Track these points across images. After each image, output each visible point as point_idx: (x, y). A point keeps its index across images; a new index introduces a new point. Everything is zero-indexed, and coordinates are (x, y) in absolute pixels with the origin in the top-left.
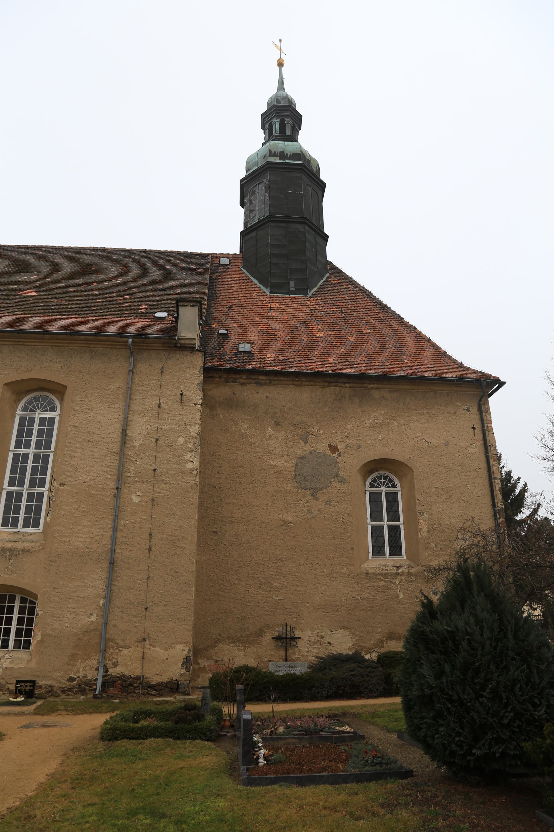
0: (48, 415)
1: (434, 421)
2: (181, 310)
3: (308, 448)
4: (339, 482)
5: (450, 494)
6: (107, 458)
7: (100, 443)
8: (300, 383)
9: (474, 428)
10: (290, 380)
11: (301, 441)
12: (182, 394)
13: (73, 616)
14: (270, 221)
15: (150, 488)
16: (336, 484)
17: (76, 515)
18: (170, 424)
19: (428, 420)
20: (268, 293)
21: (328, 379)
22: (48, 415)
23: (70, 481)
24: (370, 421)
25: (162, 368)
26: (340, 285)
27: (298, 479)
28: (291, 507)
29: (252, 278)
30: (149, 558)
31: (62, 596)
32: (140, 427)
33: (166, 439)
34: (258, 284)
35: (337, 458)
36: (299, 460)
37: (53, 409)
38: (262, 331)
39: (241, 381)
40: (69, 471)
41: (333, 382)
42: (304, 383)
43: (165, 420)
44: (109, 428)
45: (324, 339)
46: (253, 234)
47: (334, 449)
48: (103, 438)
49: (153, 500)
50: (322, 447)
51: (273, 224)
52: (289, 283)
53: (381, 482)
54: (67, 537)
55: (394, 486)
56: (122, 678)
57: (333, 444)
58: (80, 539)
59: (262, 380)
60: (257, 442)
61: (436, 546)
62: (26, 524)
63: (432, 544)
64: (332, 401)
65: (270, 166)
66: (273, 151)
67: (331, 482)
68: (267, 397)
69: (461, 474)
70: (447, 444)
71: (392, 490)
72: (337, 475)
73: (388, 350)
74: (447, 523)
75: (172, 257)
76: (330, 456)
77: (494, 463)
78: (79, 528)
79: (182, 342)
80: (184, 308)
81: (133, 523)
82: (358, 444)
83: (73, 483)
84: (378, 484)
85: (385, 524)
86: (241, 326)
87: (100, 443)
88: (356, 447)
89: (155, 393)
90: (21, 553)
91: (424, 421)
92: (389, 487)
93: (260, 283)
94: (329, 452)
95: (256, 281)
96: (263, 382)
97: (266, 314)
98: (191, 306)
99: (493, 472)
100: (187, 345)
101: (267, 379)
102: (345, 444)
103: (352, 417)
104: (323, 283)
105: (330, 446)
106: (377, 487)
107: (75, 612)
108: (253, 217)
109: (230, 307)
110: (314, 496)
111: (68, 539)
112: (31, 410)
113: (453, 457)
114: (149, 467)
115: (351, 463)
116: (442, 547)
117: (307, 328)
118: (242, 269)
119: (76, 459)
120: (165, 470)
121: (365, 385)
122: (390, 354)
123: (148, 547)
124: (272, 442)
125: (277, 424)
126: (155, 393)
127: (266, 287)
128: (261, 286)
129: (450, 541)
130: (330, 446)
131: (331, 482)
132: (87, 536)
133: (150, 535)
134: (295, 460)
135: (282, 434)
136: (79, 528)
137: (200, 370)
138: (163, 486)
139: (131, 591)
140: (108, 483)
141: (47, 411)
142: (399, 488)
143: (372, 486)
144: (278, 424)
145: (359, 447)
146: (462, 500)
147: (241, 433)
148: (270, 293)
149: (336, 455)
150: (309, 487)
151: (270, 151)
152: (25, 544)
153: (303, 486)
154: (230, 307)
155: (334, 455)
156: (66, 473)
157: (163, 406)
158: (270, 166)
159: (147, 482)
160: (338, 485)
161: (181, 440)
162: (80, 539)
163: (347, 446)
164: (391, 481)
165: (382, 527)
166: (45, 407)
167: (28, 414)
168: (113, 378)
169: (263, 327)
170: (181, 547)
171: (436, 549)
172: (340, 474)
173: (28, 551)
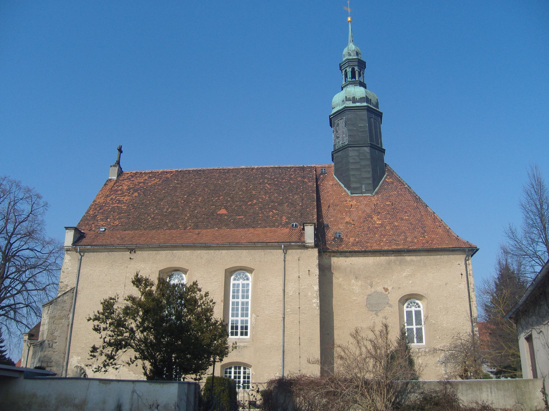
0: (246, 282)
1: (440, 271)
2: (306, 227)
3: (373, 290)
4: (389, 307)
5: (447, 311)
6: (277, 303)
7: (273, 296)
8: (367, 255)
9: (462, 274)
10: (362, 254)
11: (369, 286)
12: (309, 271)
13: (268, 374)
14: (349, 147)
15: (298, 316)
16: (387, 308)
17: (265, 330)
18: (304, 285)
19: (436, 271)
20: (350, 194)
21: (382, 253)
22: (246, 282)
23: (261, 315)
24: (405, 274)
25: (299, 258)
26: (392, 183)
27: (368, 306)
28: (365, 321)
29: (340, 183)
30: (125, 283)
31: (263, 366)
32: (291, 289)
33: (303, 293)
34: (344, 187)
35: (388, 294)
36: (368, 297)
37: (248, 279)
38: (347, 222)
39: (337, 256)
40: (260, 310)
41: (385, 254)
42: (369, 255)
43: (302, 283)
44: (276, 288)
45: (382, 225)
46: (339, 154)
47: (386, 290)
48: (274, 294)
49: (299, 322)
50: (380, 289)
51: (350, 149)
52: (362, 187)
53: (412, 305)
54: (262, 340)
55: (419, 307)
56: (321, 373)
57: (386, 287)
58: (268, 341)
59: (348, 255)
60: (347, 288)
61: (439, 338)
62: (242, 334)
63: (438, 337)
64: (385, 264)
65: (346, 109)
66: (348, 97)
67: (385, 307)
68: (351, 264)
69: (453, 300)
70: (446, 284)
71: (418, 309)
72: (388, 303)
73: (417, 230)
74: (445, 326)
75: (293, 171)
76: (384, 293)
77: (472, 293)
78: (267, 336)
79: (307, 244)
80: (307, 226)
81: (291, 332)
82: (399, 287)
83: (263, 315)
84: (411, 306)
85: (414, 327)
86: (335, 220)
87: (273, 296)
88: (397, 288)
89: (296, 271)
90: (243, 347)
91: (434, 272)
92: (416, 307)
93: (345, 187)
94: (384, 292)
95: (343, 185)
96: (348, 256)
97: (349, 210)
98: (310, 225)
99: (472, 298)
100: (310, 246)
101: (350, 255)
102: (392, 287)
103: (396, 272)
104: (383, 183)
105: (384, 288)
106: (410, 308)
107: (269, 373)
108: (339, 142)
109: (329, 206)
110: (376, 314)
111: (263, 341)
112: (237, 280)
113: (450, 291)
114: (296, 306)
115: (394, 297)
116: (443, 338)
117: (372, 218)
118: (334, 176)
119: (263, 304)
120: (304, 308)
121: (402, 254)
122: (418, 233)
123: (299, 343)
124: (355, 287)
125: (356, 278)
126: (296, 271)
127: (349, 190)
128: (346, 189)
129: (447, 335)
130: (384, 288)
131: (385, 307)
132: (271, 339)
133: (300, 338)
134: (366, 296)
135: (360, 283)
136: (267, 336)
137: (317, 257)
138: (304, 315)
139: (293, 363)
140: (278, 315)
141: (245, 280)
142: (422, 307)
143: (407, 307)
144: (357, 278)
145: (399, 288)
146: (454, 314)
147: (338, 283)
148: (352, 194)
149: (387, 293)
150: (374, 310)
151: (346, 97)
152: (245, 344)
153: (371, 310)
154: (329, 206)
155: (386, 293)
156: (259, 311)
157: (300, 276)
158: (346, 109)
159: (296, 314)
160: (389, 308)
161: (310, 294)
162: (268, 341)
163: (393, 288)
164: (417, 304)
165: (413, 329)
166: (244, 278)
167: (236, 282)
168: (276, 264)
169: (348, 219)
170: (313, 343)
171: (440, 339)
172: (389, 302)
173: (246, 346)
